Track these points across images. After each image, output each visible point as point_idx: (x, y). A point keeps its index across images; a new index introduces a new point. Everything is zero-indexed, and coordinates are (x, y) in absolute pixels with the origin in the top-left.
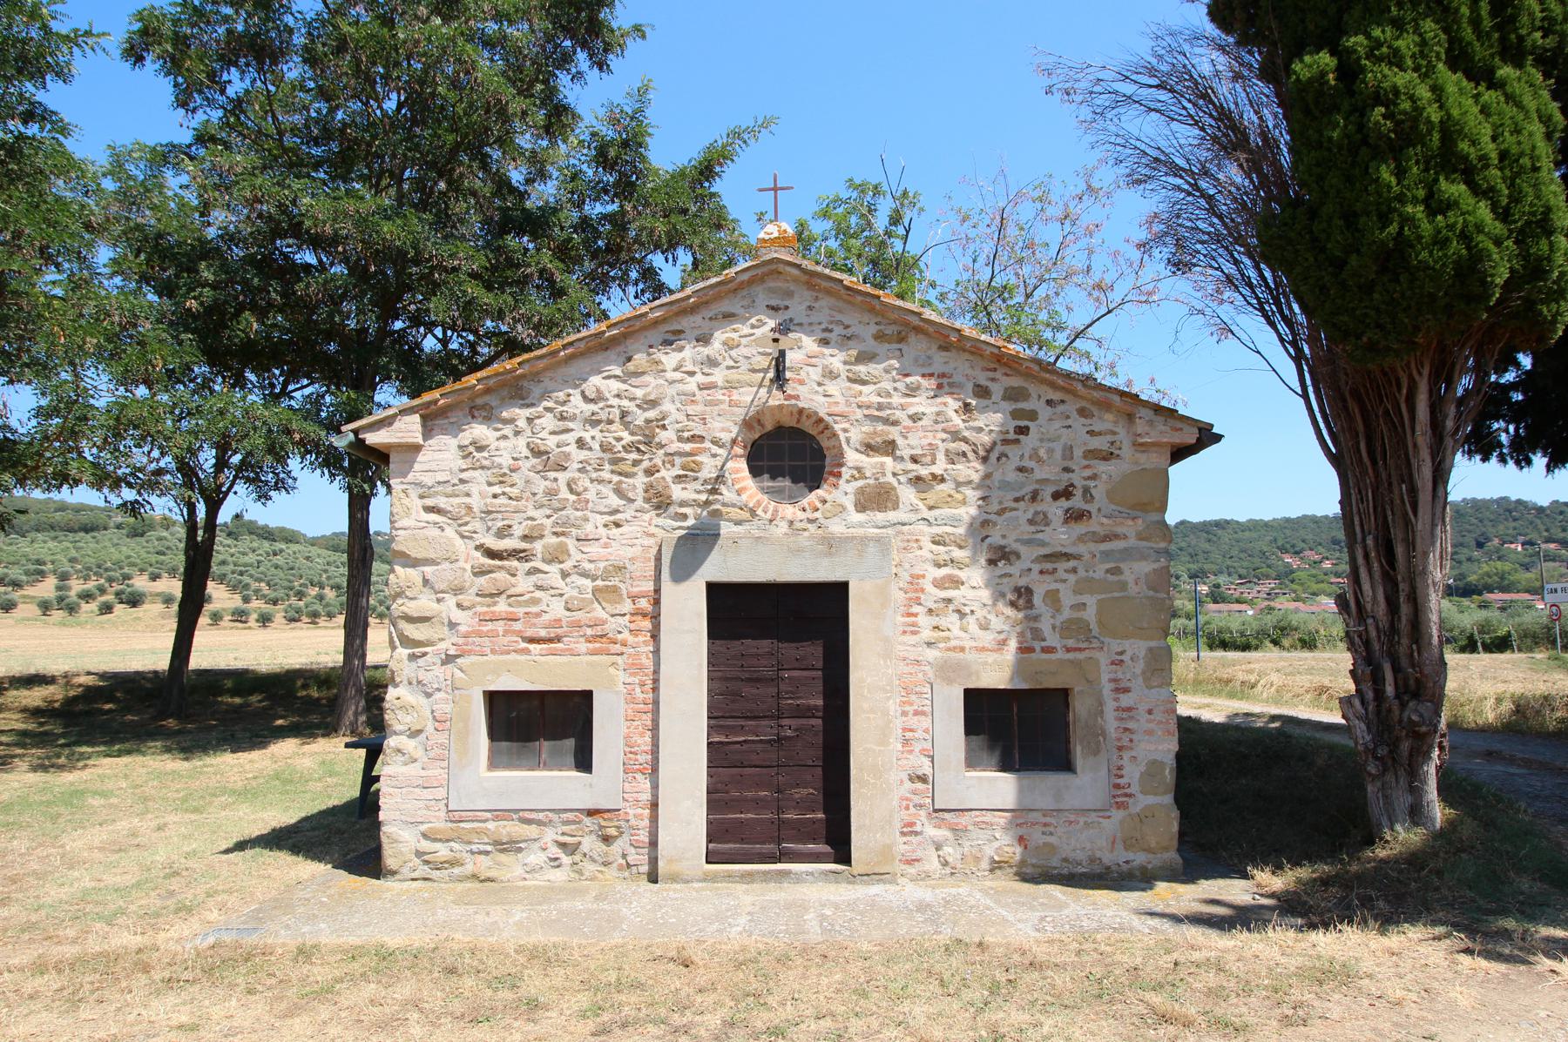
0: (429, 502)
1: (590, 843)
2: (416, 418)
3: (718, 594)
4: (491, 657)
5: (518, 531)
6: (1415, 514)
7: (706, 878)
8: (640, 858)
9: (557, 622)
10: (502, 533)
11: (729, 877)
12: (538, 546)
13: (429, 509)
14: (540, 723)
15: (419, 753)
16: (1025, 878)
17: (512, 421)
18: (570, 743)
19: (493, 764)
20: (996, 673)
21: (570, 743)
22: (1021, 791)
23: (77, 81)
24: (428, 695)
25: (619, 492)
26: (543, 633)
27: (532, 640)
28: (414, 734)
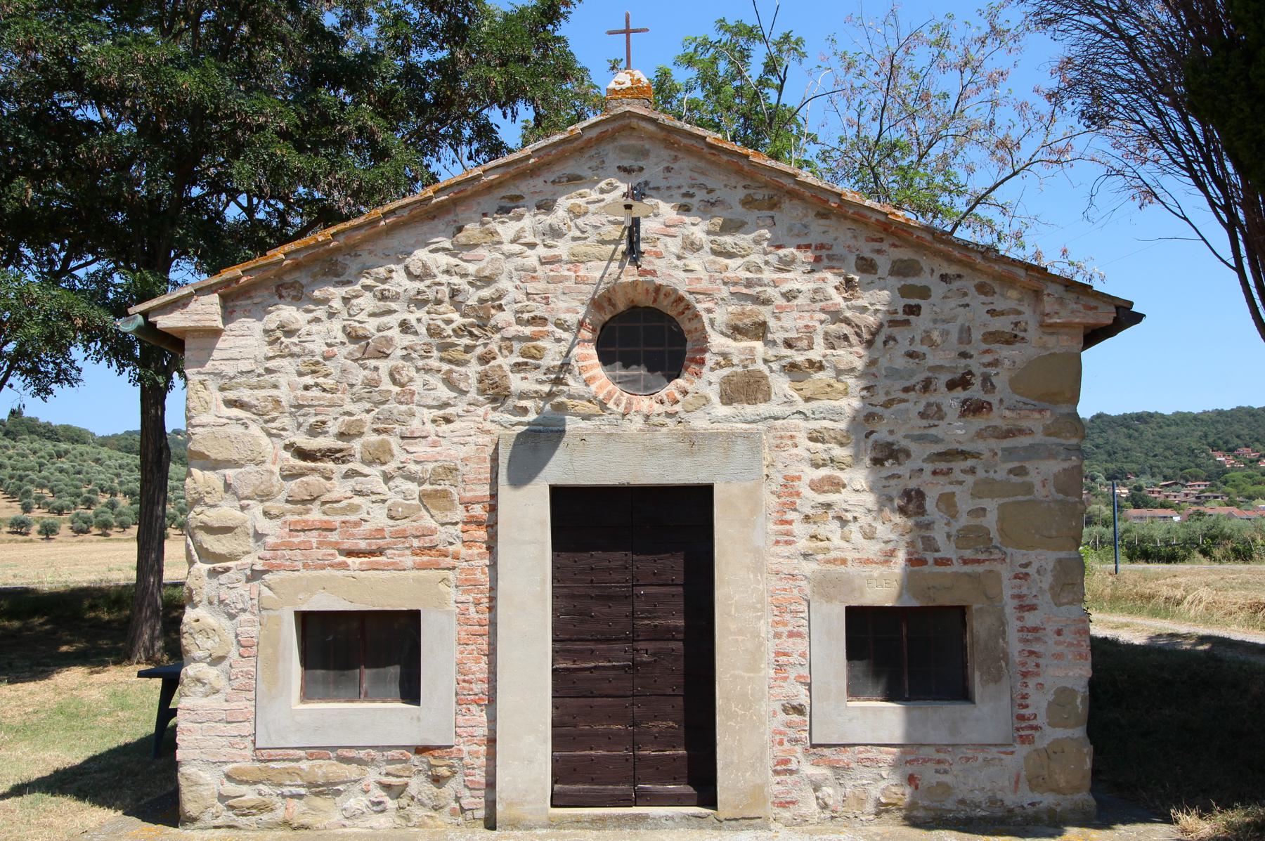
0: (231, 395)
2: (215, 298)
5: (333, 428)
7: (552, 824)
8: (475, 801)
10: (314, 431)
13: (231, 403)
14: (361, 648)
15: (222, 683)
22: (910, 723)
24: (232, 617)
27: (350, 553)
28: (216, 661)
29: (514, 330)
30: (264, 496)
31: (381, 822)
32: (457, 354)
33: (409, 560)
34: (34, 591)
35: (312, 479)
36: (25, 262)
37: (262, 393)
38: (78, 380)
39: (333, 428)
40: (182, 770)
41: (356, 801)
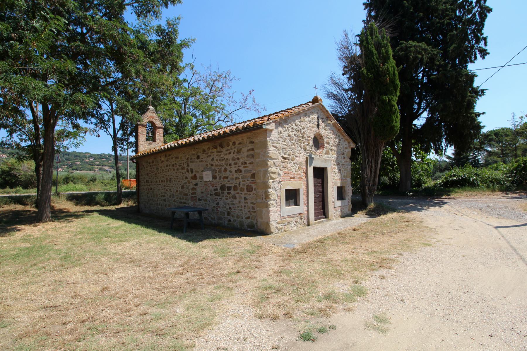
0: (274, 145)
1: (299, 220)
2: (274, 124)
3: (315, 168)
4: (286, 182)
5: (287, 154)
6: (101, 212)
7: (315, 224)
8: (306, 222)
9: (294, 174)
10: (285, 154)
11: (319, 222)
12: (290, 157)
13: (274, 146)
14: (292, 196)
15: (275, 204)
16: (341, 217)
17: (285, 128)
18: (293, 200)
19: (286, 206)
20: (339, 185)
21: (293, 200)
22: (341, 203)
23: (362, 5)
24: (276, 191)
25: (300, 147)
26: (293, 176)
27: (291, 178)
28: (274, 200)
29: (307, 138)
30: (280, 166)
31: (295, 228)
32: (301, 141)
33: (298, 179)
34: (167, 233)
35: (286, 163)
36: (24, 137)
37: (278, 145)
38: (473, 62)
39: (287, 154)
40: (271, 223)
41: (293, 225)
